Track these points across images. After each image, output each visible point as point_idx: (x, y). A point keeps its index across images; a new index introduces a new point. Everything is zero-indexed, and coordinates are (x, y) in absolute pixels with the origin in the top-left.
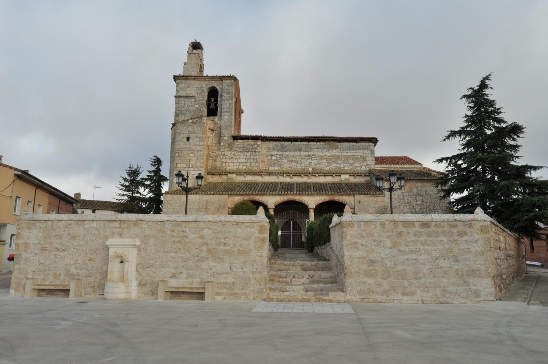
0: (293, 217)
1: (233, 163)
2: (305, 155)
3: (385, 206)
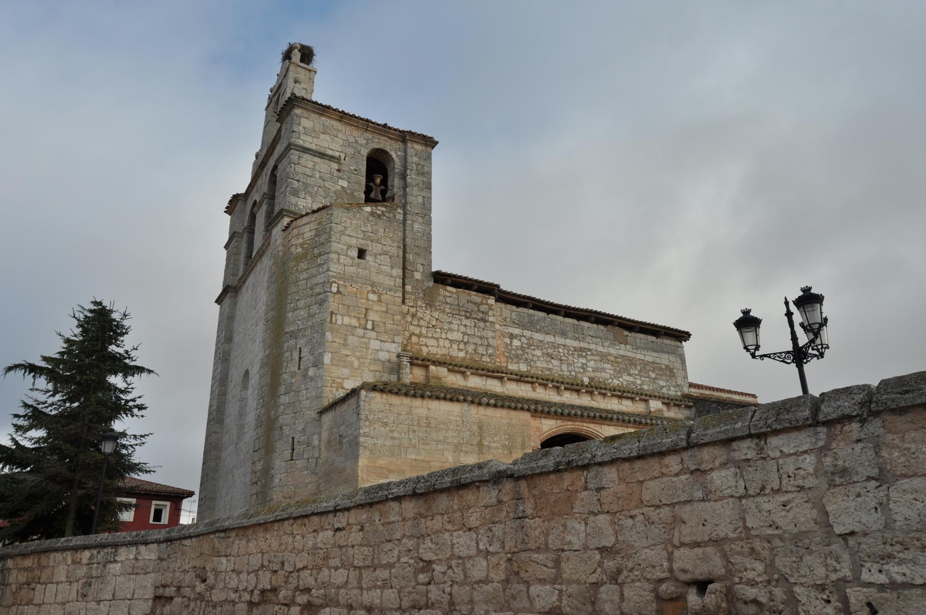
2: (574, 347)
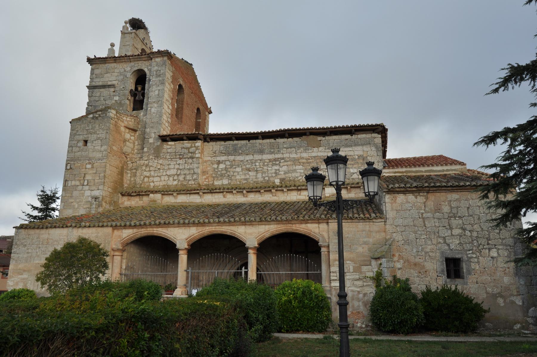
1: (160, 177)
3: (387, 240)
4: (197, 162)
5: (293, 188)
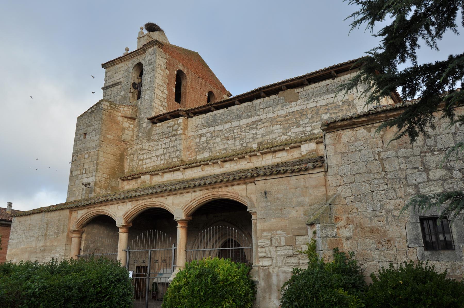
0: (232, 236)
4: (180, 139)
5: (266, 150)
